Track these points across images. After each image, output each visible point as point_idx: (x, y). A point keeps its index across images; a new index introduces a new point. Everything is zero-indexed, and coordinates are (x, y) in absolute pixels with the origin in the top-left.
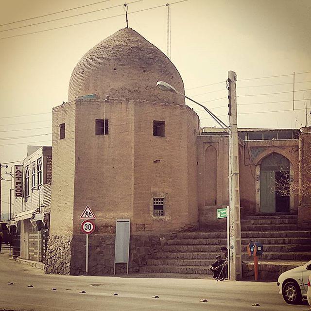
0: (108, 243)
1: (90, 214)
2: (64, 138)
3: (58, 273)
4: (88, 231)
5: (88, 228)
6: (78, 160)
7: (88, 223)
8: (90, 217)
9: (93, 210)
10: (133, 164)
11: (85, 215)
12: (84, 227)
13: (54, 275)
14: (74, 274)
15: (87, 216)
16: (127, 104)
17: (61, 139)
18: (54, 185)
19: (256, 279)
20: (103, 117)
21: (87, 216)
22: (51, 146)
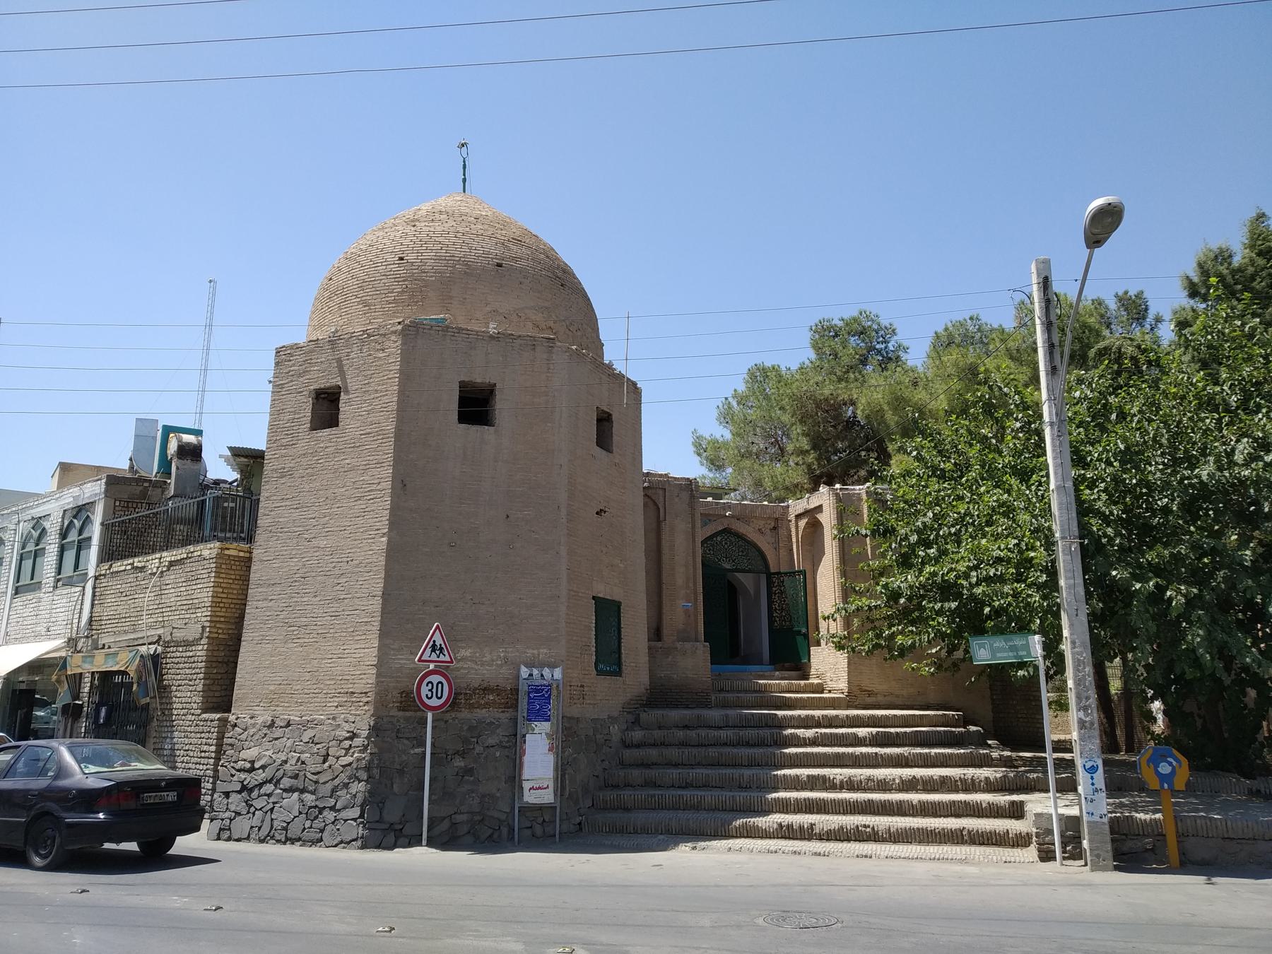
0: (491, 741)
1: (441, 649)
2: (337, 426)
3: (293, 841)
4: (434, 702)
5: (433, 695)
6: (401, 484)
7: (435, 679)
8: (442, 658)
9: (449, 632)
10: (564, 512)
11: (429, 650)
12: (425, 690)
13: (271, 849)
14: (379, 846)
15: (434, 657)
16: (550, 352)
17: (313, 428)
18: (1196, 260)
19: (424, 842)
20: (479, 377)
21: (434, 657)
22: (264, 449)
